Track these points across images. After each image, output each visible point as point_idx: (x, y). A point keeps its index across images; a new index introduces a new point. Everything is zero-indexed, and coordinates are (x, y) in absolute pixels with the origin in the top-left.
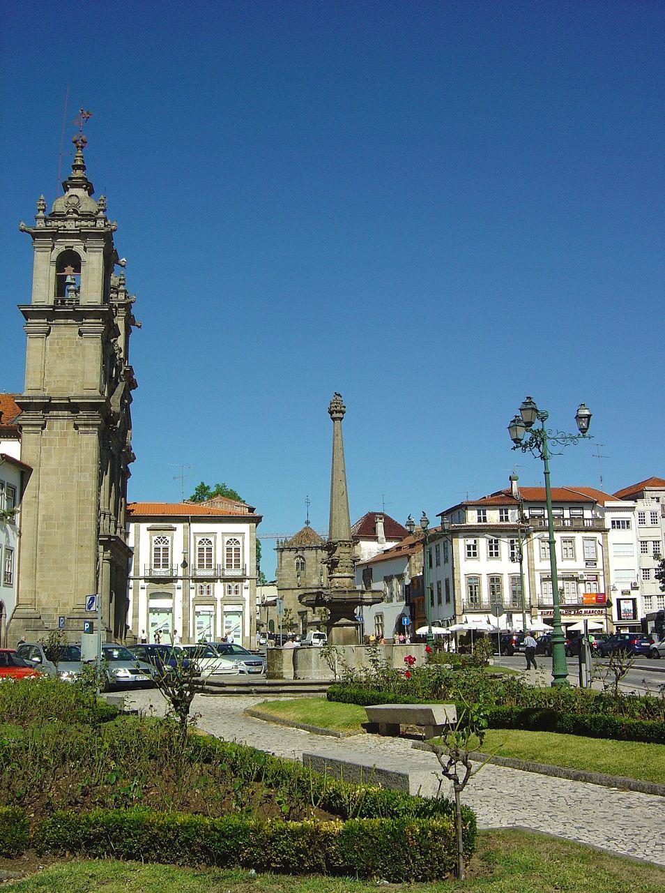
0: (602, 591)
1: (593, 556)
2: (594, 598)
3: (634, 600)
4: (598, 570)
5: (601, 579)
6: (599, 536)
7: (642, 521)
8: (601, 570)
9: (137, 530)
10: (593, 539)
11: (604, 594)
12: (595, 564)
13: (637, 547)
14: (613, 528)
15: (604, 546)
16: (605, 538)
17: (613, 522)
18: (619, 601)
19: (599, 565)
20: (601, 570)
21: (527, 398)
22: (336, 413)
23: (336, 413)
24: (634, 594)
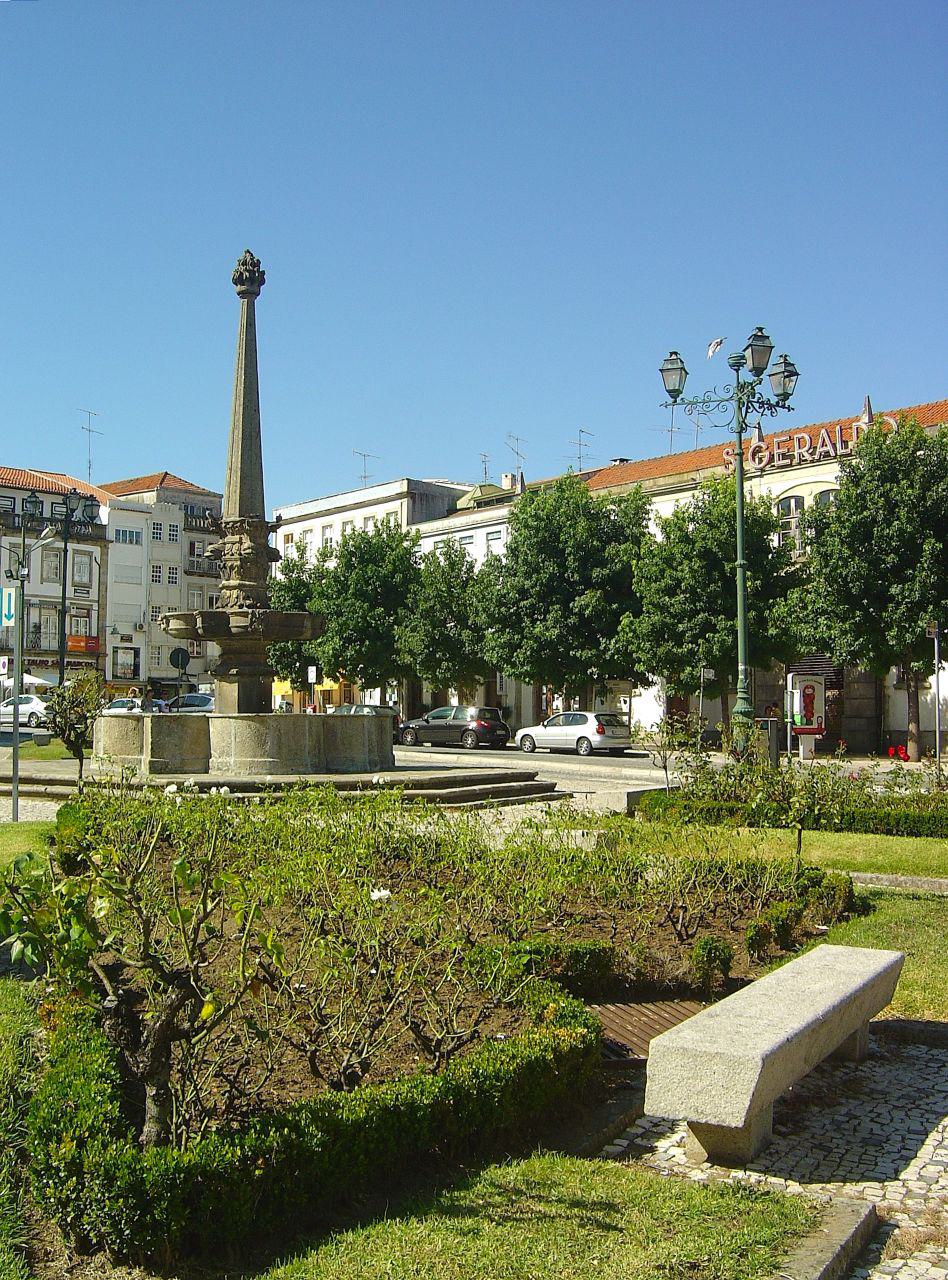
0: (94, 634)
1: (85, 580)
2: (83, 644)
3: (137, 652)
4: (90, 601)
5: (94, 614)
6: (96, 550)
7: (157, 536)
8: (94, 601)
9: (24, 770)
10: (90, 554)
11: (388, 765)
12: (88, 592)
13: (146, 575)
14: (117, 540)
15: (103, 566)
16: (104, 554)
17: (118, 531)
18: (115, 650)
19: (94, 594)
20: (94, 601)
21: (671, 354)
22: (250, 280)
23: (250, 280)
24: (138, 641)
